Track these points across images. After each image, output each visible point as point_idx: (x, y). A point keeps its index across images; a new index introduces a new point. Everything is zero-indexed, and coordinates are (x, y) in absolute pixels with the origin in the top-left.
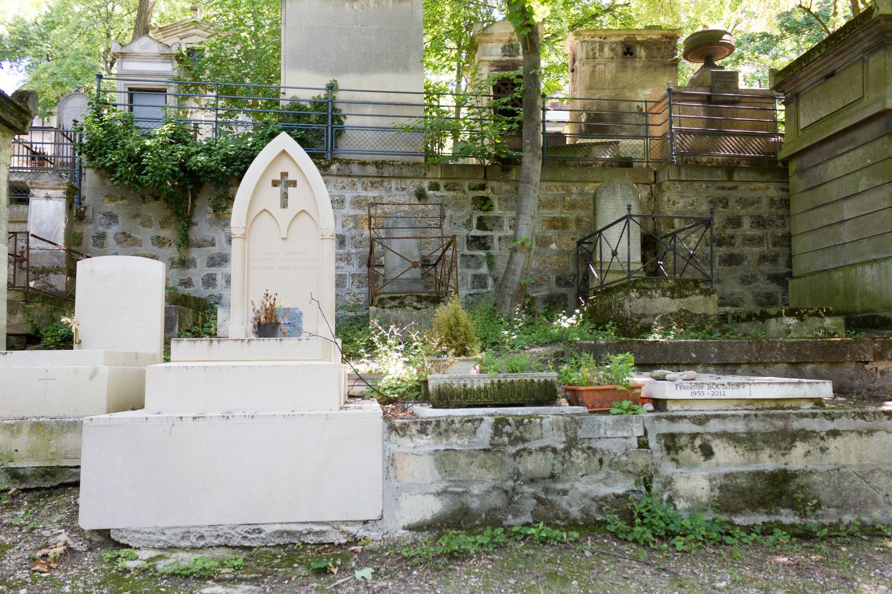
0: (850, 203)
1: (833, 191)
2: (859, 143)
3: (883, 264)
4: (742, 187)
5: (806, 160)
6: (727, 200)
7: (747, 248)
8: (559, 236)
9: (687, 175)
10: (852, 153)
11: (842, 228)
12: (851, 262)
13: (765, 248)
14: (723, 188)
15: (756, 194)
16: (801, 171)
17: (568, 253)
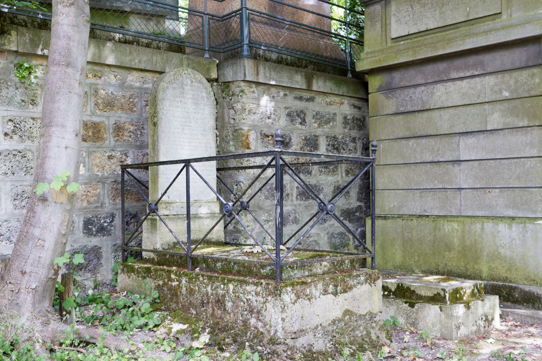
0: (471, 140)
1: (443, 122)
2: (489, 70)
3: (530, 226)
4: (319, 99)
5: (397, 77)
6: (305, 114)
7: (323, 177)
8: (89, 154)
9: (266, 77)
10: (477, 79)
11: (456, 168)
12: (470, 214)
13: (339, 178)
14: (301, 98)
15: (332, 109)
16: (388, 90)
17: (102, 181)
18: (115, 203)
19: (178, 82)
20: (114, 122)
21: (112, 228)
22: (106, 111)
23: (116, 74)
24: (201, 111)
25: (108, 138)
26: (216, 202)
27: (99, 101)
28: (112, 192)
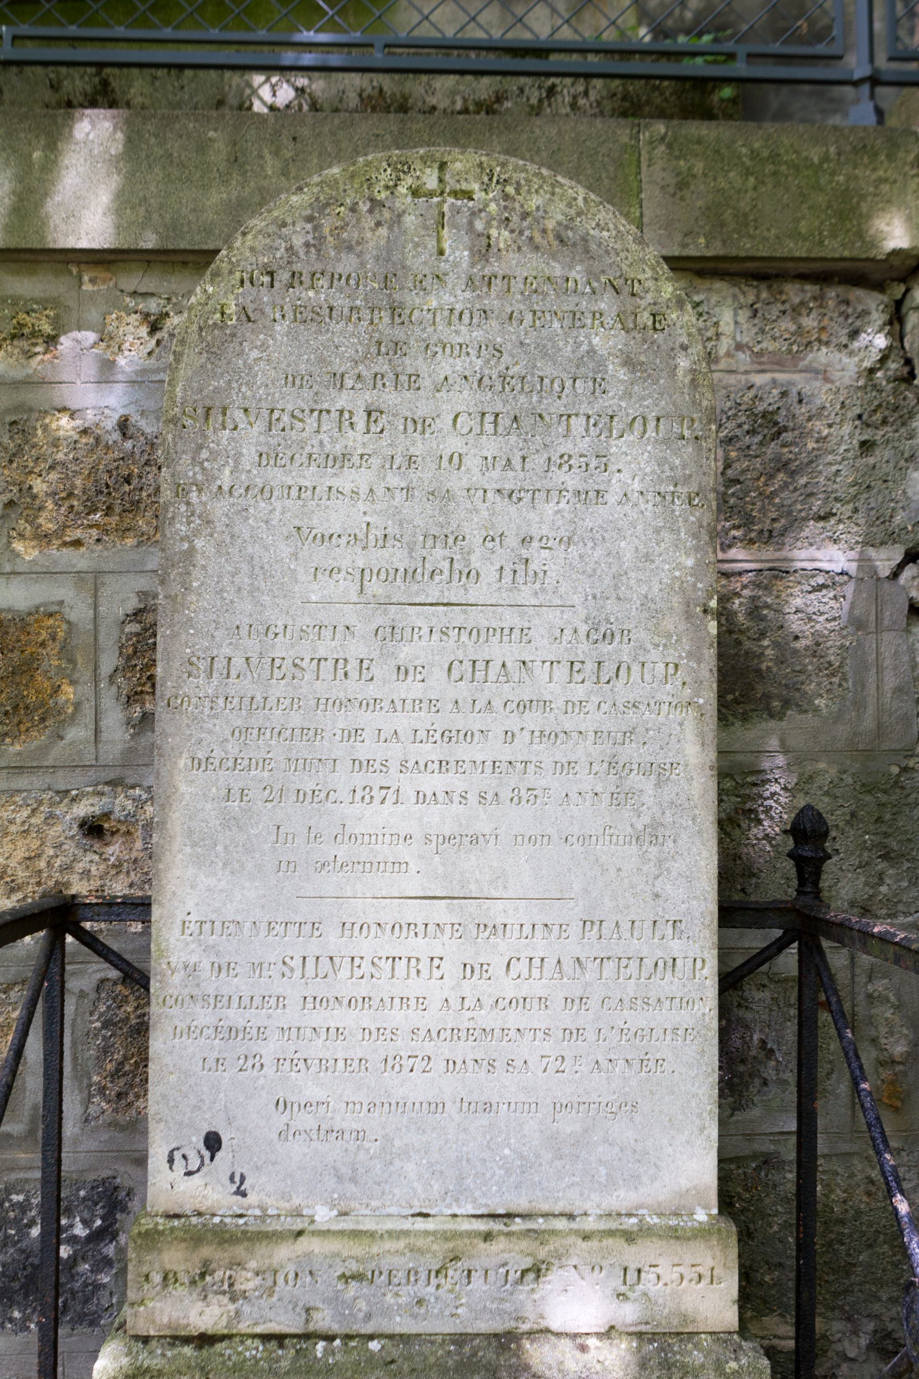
18: (124, 1118)
19: (347, 264)
20: (133, 604)
21: (105, 1279)
22: (77, 543)
23: (153, 305)
24: (572, 481)
25: (88, 710)
26: (701, 1233)
27: (39, 486)
28: (105, 1051)
